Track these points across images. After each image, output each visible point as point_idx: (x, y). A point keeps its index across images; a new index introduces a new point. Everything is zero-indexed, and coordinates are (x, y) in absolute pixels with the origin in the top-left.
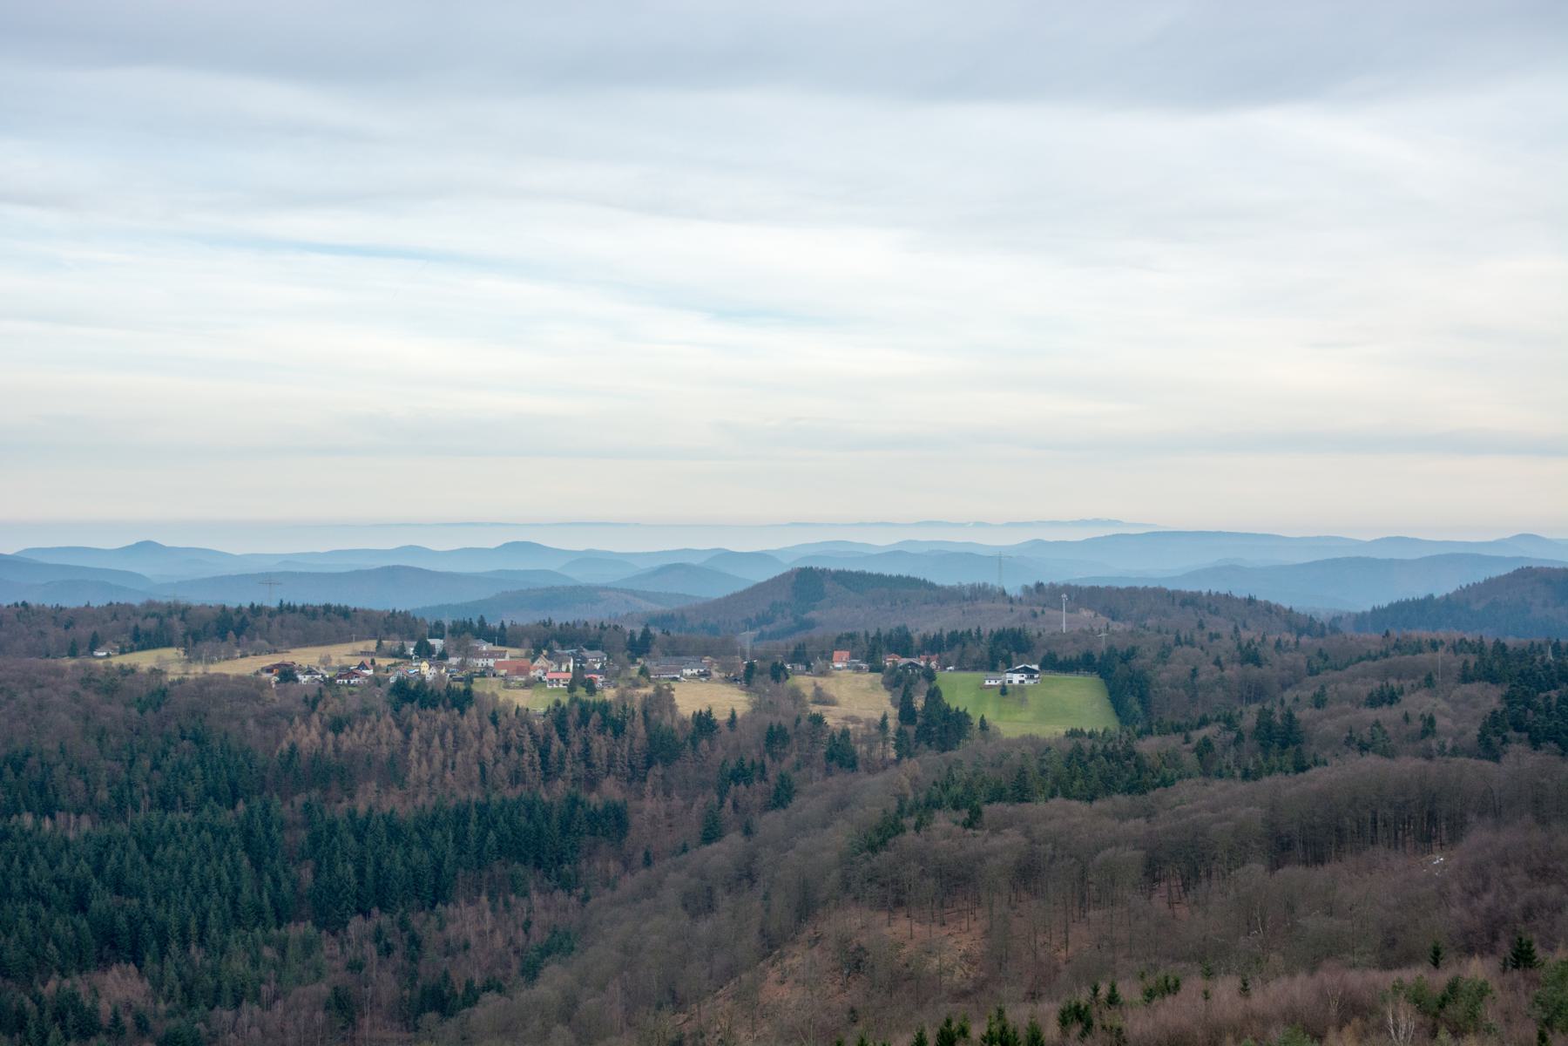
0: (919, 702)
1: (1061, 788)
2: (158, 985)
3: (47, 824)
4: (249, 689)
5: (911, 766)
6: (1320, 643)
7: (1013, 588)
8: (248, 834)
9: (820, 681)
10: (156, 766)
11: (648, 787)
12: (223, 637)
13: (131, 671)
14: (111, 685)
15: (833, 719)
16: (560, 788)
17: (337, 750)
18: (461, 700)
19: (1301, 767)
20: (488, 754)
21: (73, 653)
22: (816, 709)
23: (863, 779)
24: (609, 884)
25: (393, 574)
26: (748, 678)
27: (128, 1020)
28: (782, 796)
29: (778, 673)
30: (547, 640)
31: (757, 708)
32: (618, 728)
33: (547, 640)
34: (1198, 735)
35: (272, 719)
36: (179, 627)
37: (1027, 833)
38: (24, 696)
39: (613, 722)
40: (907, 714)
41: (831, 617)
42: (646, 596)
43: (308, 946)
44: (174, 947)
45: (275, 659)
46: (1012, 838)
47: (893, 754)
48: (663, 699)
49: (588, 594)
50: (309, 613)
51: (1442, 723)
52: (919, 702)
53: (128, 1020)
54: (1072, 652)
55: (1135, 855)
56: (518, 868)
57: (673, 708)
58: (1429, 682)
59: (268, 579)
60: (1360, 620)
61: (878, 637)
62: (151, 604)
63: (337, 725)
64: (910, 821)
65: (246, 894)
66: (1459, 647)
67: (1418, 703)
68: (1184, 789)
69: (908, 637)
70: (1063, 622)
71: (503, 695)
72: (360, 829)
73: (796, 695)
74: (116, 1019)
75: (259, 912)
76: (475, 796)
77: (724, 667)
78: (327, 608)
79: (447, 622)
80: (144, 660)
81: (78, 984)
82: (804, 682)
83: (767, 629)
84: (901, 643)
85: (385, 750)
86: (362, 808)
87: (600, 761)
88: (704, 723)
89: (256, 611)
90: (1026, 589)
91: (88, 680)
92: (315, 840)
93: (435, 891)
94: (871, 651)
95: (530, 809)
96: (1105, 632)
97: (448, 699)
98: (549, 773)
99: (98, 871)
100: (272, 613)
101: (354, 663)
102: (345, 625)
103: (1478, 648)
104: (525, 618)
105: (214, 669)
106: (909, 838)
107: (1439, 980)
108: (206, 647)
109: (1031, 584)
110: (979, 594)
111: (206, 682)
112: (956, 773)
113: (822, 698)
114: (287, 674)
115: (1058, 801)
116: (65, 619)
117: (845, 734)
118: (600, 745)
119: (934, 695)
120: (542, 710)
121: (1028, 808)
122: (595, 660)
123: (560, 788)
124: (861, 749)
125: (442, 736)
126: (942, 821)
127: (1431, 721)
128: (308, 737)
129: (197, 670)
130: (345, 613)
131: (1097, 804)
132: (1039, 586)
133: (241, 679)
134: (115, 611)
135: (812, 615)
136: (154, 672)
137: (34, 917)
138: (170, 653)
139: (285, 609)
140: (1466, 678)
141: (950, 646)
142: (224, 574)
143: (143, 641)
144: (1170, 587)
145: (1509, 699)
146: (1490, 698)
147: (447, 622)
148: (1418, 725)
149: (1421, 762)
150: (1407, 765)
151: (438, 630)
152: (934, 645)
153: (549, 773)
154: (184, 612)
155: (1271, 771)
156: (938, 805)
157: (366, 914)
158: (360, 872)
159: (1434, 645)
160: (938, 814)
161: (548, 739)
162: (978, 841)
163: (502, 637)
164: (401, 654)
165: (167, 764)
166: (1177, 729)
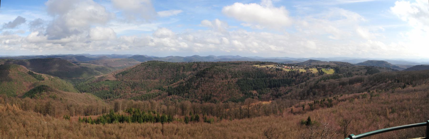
0: (320, 71)
1: (332, 78)
2: (258, 92)
3: (249, 78)
4: (265, 68)
5: (320, 76)
6: (353, 66)
7: (328, 62)
8: (264, 80)
9: (312, 69)
10: (257, 74)
11: (297, 78)
12: (263, 64)
13: (255, 67)
14: (254, 68)
15: (313, 72)
16: (290, 78)
17: (272, 74)
18: (282, 70)
19: (352, 76)
20: (284, 75)
21: (251, 65)
22: (312, 71)
23: (315, 78)
24: (294, 86)
25: (276, 59)
26: (305, 69)
27: (255, 95)
28: (308, 79)
29: (308, 68)
30: (289, 65)
31: (307, 71)
32: (295, 73)
33: (289, 65)
34: (343, 74)
35: (267, 71)
36: (259, 63)
37: (330, 82)
38: (248, 68)
39: (294, 72)
40: (319, 72)
41: (313, 64)
42: (297, 62)
43: (269, 90)
44: (259, 89)
45: (266, 66)
46: (328, 83)
47: (318, 75)
48: (298, 71)
49: (292, 61)
50: (269, 62)
51: (363, 73)
52: (320, 71)
53: (255, 95)
54: (333, 67)
55: (338, 84)
56: (286, 84)
57: (299, 71)
58: (362, 69)
59: (266, 60)
60: (356, 64)
61: (317, 65)
62: (257, 61)
63: (271, 72)
64: (319, 81)
65: (264, 85)
66: (364, 66)
67: (361, 71)
68: (342, 78)
69: (319, 65)
70: (333, 64)
71: (285, 70)
72: (274, 81)
73: (310, 70)
74: (254, 95)
75: (265, 87)
76: (283, 78)
77: (304, 68)
78: (271, 62)
79: (280, 63)
80: (256, 66)
81: (252, 91)
82: (310, 69)
83: (307, 65)
84: (319, 66)
85: (275, 74)
86: (273, 79)
87: (293, 76)
88: (302, 73)
89: (265, 62)
90: (329, 62)
91: (252, 67)
92: (270, 81)
93: (279, 86)
94: (316, 67)
95: (287, 80)
96: (336, 65)
97: (281, 76)
98: (289, 76)
99: (253, 83)
100: (266, 62)
101: (273, 67)
102: (272, 63)
103: (365, 67)
104: (287, 63)
105: (262, 67)
106: (319, 83)
107: (363, 94)
108: (261, 65)
109: (329, 61)
110: (325, 62)
111: (261, 68)
112: (323, 77)
113: (312, 71)
114: (267, 67)
115: (332, 79)
116: (251, 62)
117: (314, 74)
118: (293, 74)
119: (321, 70)
120: (288, 71)
121: (330, 80)
122: (293, 67)
123: (290, 78)
124: (315, 75)
125: (280, 73)
126: (322, 81)
127: (362, 73)
128: (269, 73)
129: (261, 67)
130: (272, 62)
131: (335, 80)
132: (330, 61)
133: (264, 68)
134: (254, 62)
135: (311, 63)
136: (257, 67)
137: (249, 86)
138: (258, 65)
139: (267, 62)
140: (364, 69)
141: (323, 67)
142: (255, 61)
143: (256, 64)
144: (341, 61)
145: (367, 71)
146: (366, 71)
147: (280, 63)
148: (360, 73)
149: (361, 76)
150: (360, 76)
151: (280, 64)
152: (321, 66)
153: (289, 76)
154: (260, 62)
155: (349, 77)
156: (322, 80)
157: (274, 88)
158: (273, 84)
159: (362, 66)
160: (322, 80)
161: (289, 74)
162: (325, 83)
163: (285, 65)
164: (277, 66)
165: (258, 74)
166: (342, 73)
